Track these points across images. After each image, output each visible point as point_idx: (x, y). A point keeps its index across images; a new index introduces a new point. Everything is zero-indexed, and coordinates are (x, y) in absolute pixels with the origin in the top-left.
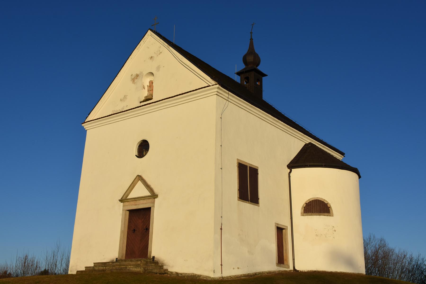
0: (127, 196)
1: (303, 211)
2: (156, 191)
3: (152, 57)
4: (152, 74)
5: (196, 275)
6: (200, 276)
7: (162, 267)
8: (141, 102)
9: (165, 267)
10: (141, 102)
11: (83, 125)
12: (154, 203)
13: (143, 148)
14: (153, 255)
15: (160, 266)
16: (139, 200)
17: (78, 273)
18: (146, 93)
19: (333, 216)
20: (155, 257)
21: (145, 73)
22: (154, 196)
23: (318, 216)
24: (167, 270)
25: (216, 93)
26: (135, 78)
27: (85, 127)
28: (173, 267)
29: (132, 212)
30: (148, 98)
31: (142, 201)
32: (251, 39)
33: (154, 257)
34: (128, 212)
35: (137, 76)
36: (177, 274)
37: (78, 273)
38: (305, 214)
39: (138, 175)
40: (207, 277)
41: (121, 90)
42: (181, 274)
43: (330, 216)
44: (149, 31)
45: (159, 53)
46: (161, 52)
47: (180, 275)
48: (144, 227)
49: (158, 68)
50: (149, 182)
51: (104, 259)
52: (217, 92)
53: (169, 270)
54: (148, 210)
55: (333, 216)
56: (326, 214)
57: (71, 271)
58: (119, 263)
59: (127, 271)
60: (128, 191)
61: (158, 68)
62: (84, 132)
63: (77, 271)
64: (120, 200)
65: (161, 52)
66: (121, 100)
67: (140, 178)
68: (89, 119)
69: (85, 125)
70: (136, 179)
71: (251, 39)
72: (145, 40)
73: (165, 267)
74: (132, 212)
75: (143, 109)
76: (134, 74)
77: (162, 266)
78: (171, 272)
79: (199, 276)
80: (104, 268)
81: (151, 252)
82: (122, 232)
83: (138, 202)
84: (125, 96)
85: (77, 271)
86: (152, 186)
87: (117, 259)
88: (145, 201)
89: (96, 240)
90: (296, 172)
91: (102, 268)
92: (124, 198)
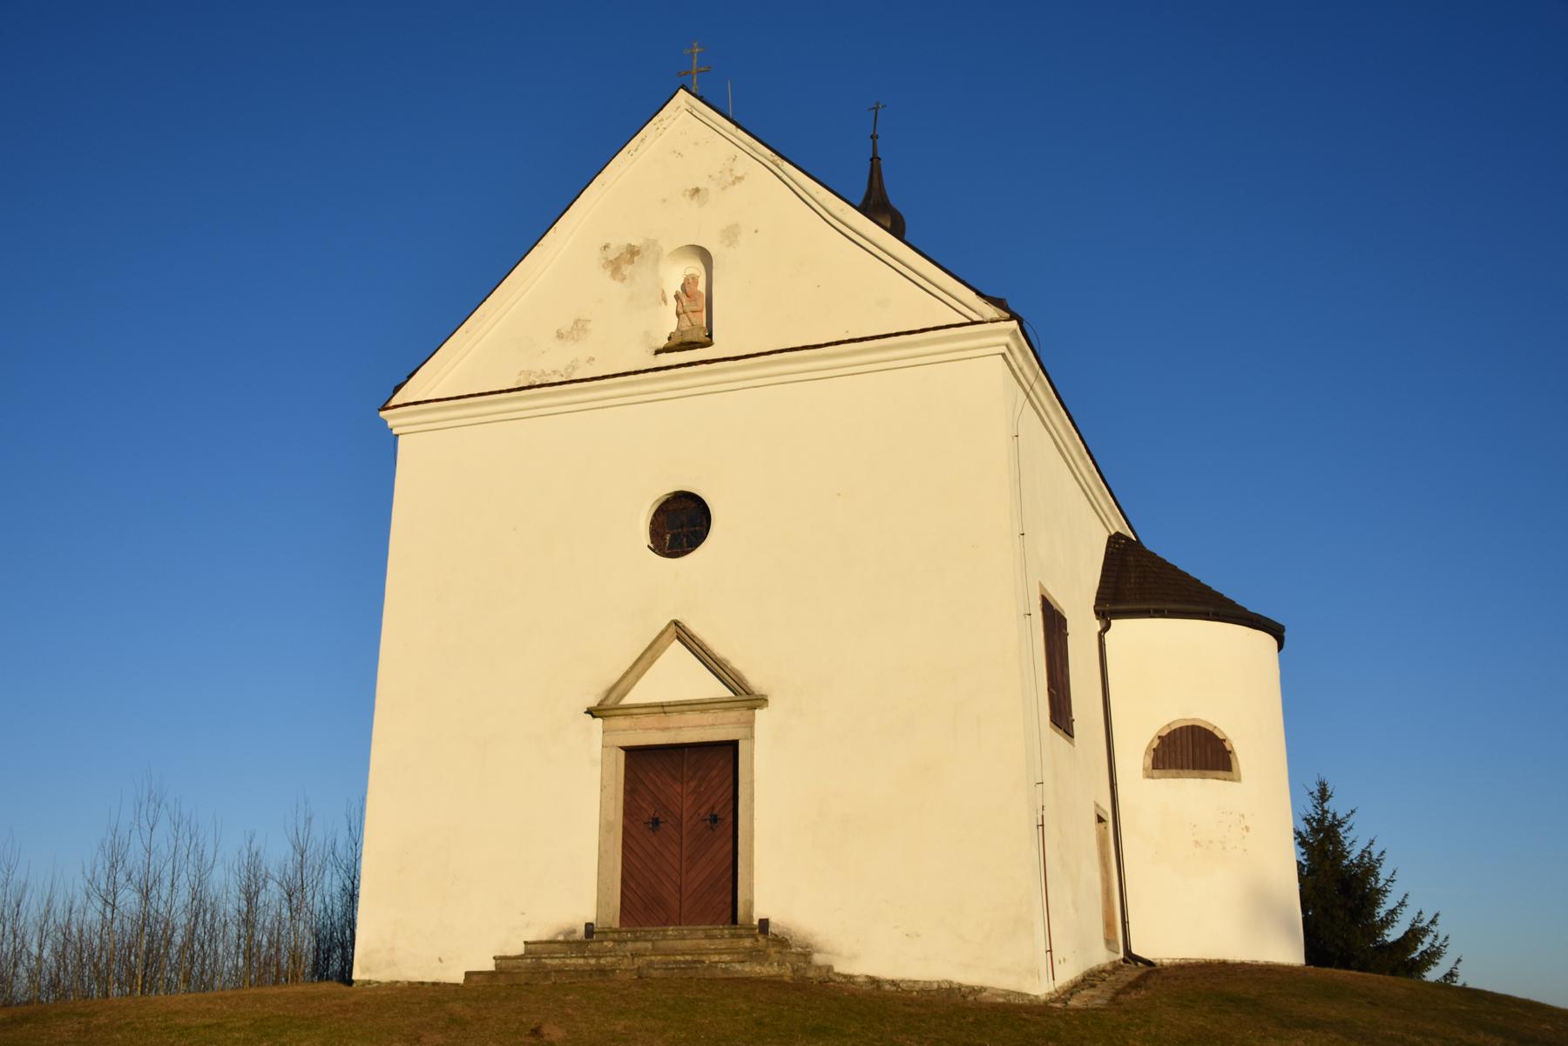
0: (623, 696)
1: (1149, 762)
2: (756, 680)
3: (697, 190)
4: (704, 255)
5: (960, 987)
6: (982, 989)
7: (806, 954)
8: (658, 352)
9: (818, 959)
10: (658, 352)
11: (382, 414)
12: (752, 728)
13: (681, 523)
14: (759, 913)
15: (798, 954)
16: (681, 712)
17: (475, 978)
18: (667, 324)
19: (1239, 780)
20: (773, 920)
21: (668, 248)
22: (747, 698)
23: (1199, 781)
24: (830, 968)
25: (1003, 349)
26: (622, 261)
27: (390, 424)
28: (854, 957)
29: (635, 755)
30: (688, 338)
31: (693, 718)
32: (875, 159)
33: (764, 923)
34: (622, 753)
35: (633, 252)
36: (875, 982)
37: (475, 978)
38: (1156, 772)
39: (676, 623)
40: (1009, 993)
41: (563, 290)
42: (893, 983)
43: (1232, 780)
44: (682, 91)
45: (730, 179)
46: (740, 179)
47: (887, 987)
48: (702, 811)
49: (731, 234)
50: (719, 649)
51: (528, 925)
52: (1007, 346)
53: (837, 969)
54: (728, 751)
55: (1239, 780)
56: (1221, 774)
57: (363, 972)
58: (649, 945)
59: (719, 974)
60: (631, 677)
61: (731, 234)
62: (391, 441)
63: (468, 974)
64: (591, 712)
65: (740, 179)
66: (560, 335)
67: (680, 632)
68: (407, 393)
69: (392, 417)
70: (667, 635)
71: (875, 159)
72: (665, 123)
73: (818, 959)
74: (635, 755)
75: (678, 377)
76: (619, 242)
77: (810, 954)
78: (845, 976)
79: (975, 991)
80: (592, 961)
81: (750, 904)
82: (605, 827)
83: (675, 720)
84: (576, 322)
85: (468, 974)
86: (738, 663)
87: (589, 929)
88: (708, 718)
89: (480, 854)
90: (1123, 629)
91: (581, 961)
92: (610, 702)
